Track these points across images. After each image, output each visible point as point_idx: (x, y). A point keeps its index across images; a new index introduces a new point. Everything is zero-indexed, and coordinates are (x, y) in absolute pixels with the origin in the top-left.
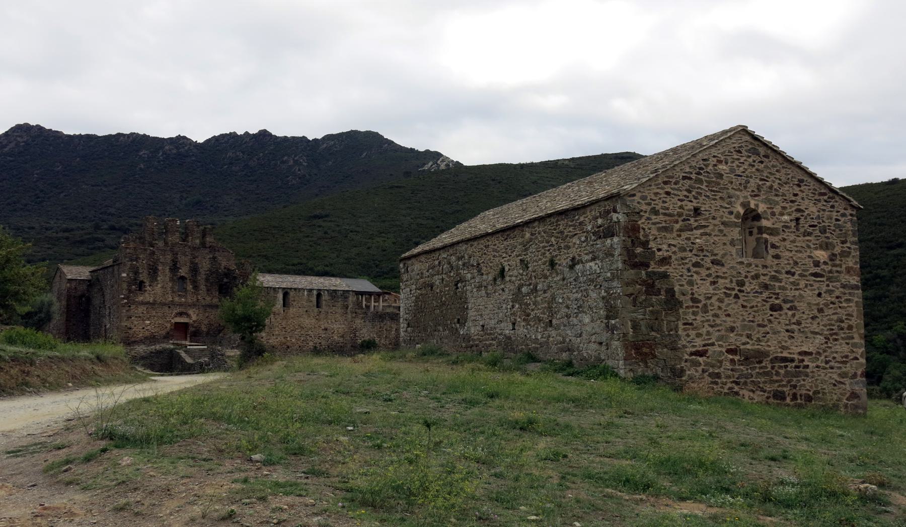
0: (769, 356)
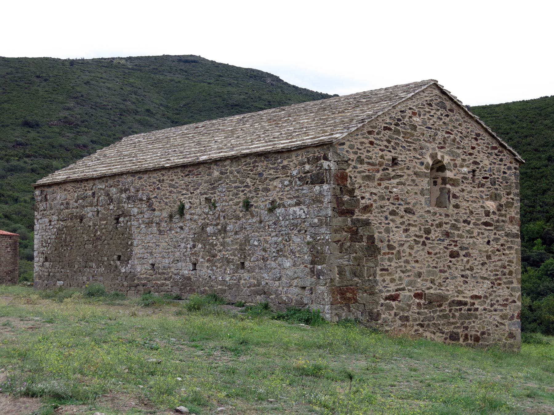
0: (447, 300)
